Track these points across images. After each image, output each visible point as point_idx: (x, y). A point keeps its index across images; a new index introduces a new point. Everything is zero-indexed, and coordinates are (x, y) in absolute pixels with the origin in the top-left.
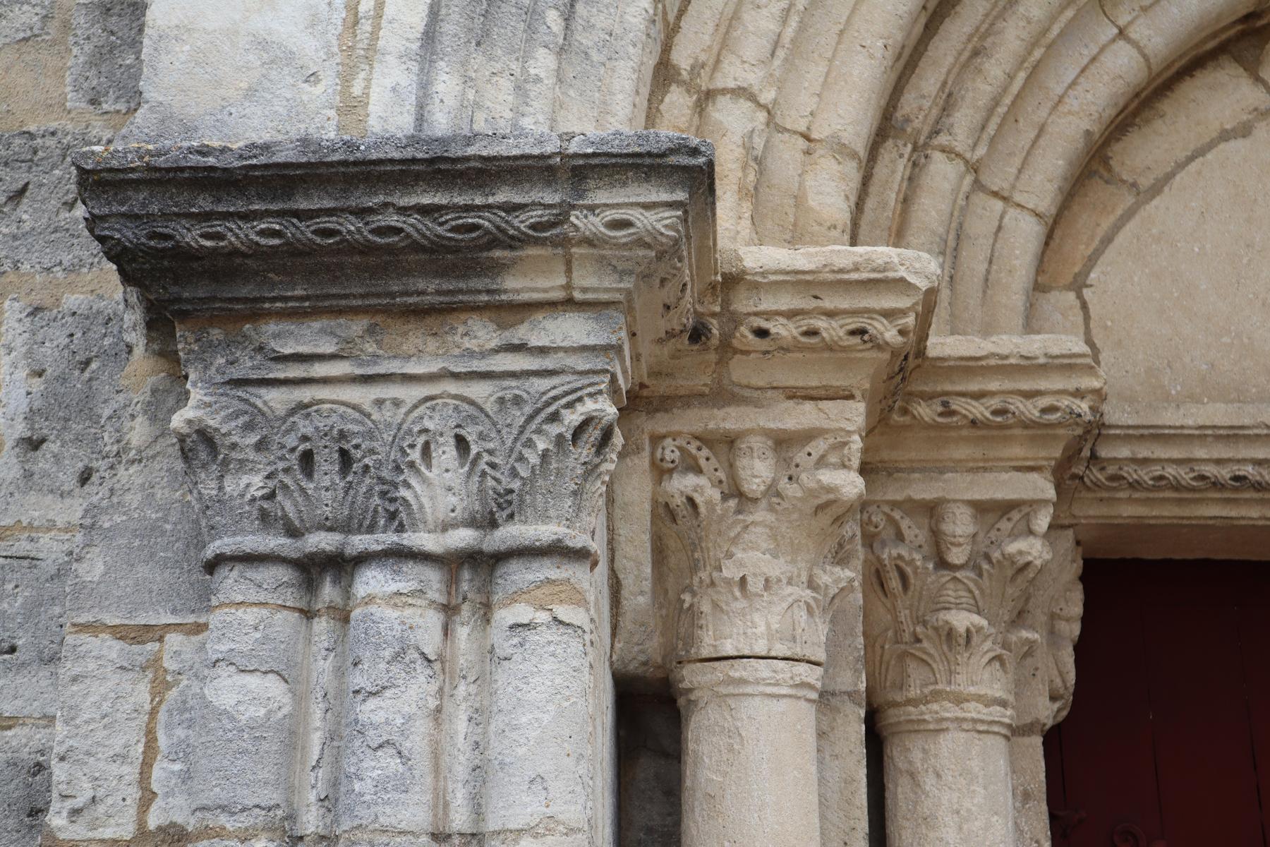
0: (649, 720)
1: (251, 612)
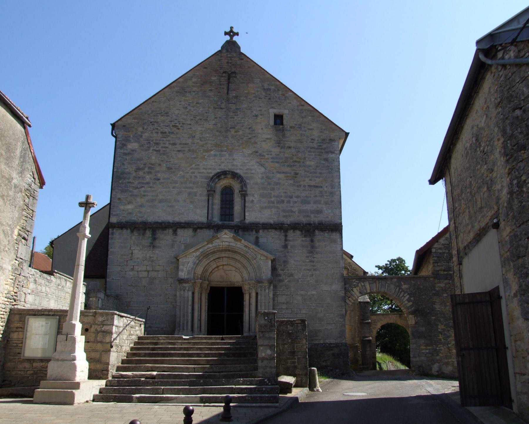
0: (193, 293)
1: (182, 291)
